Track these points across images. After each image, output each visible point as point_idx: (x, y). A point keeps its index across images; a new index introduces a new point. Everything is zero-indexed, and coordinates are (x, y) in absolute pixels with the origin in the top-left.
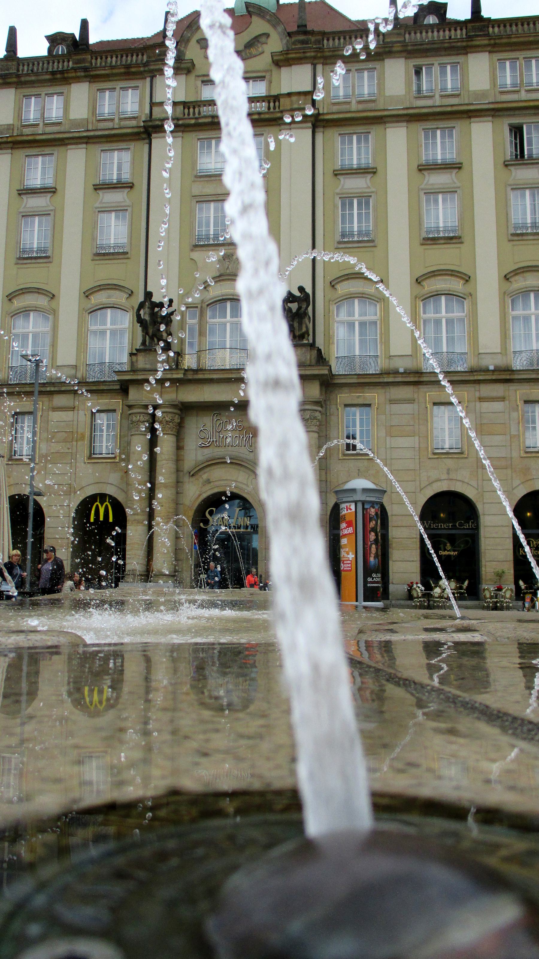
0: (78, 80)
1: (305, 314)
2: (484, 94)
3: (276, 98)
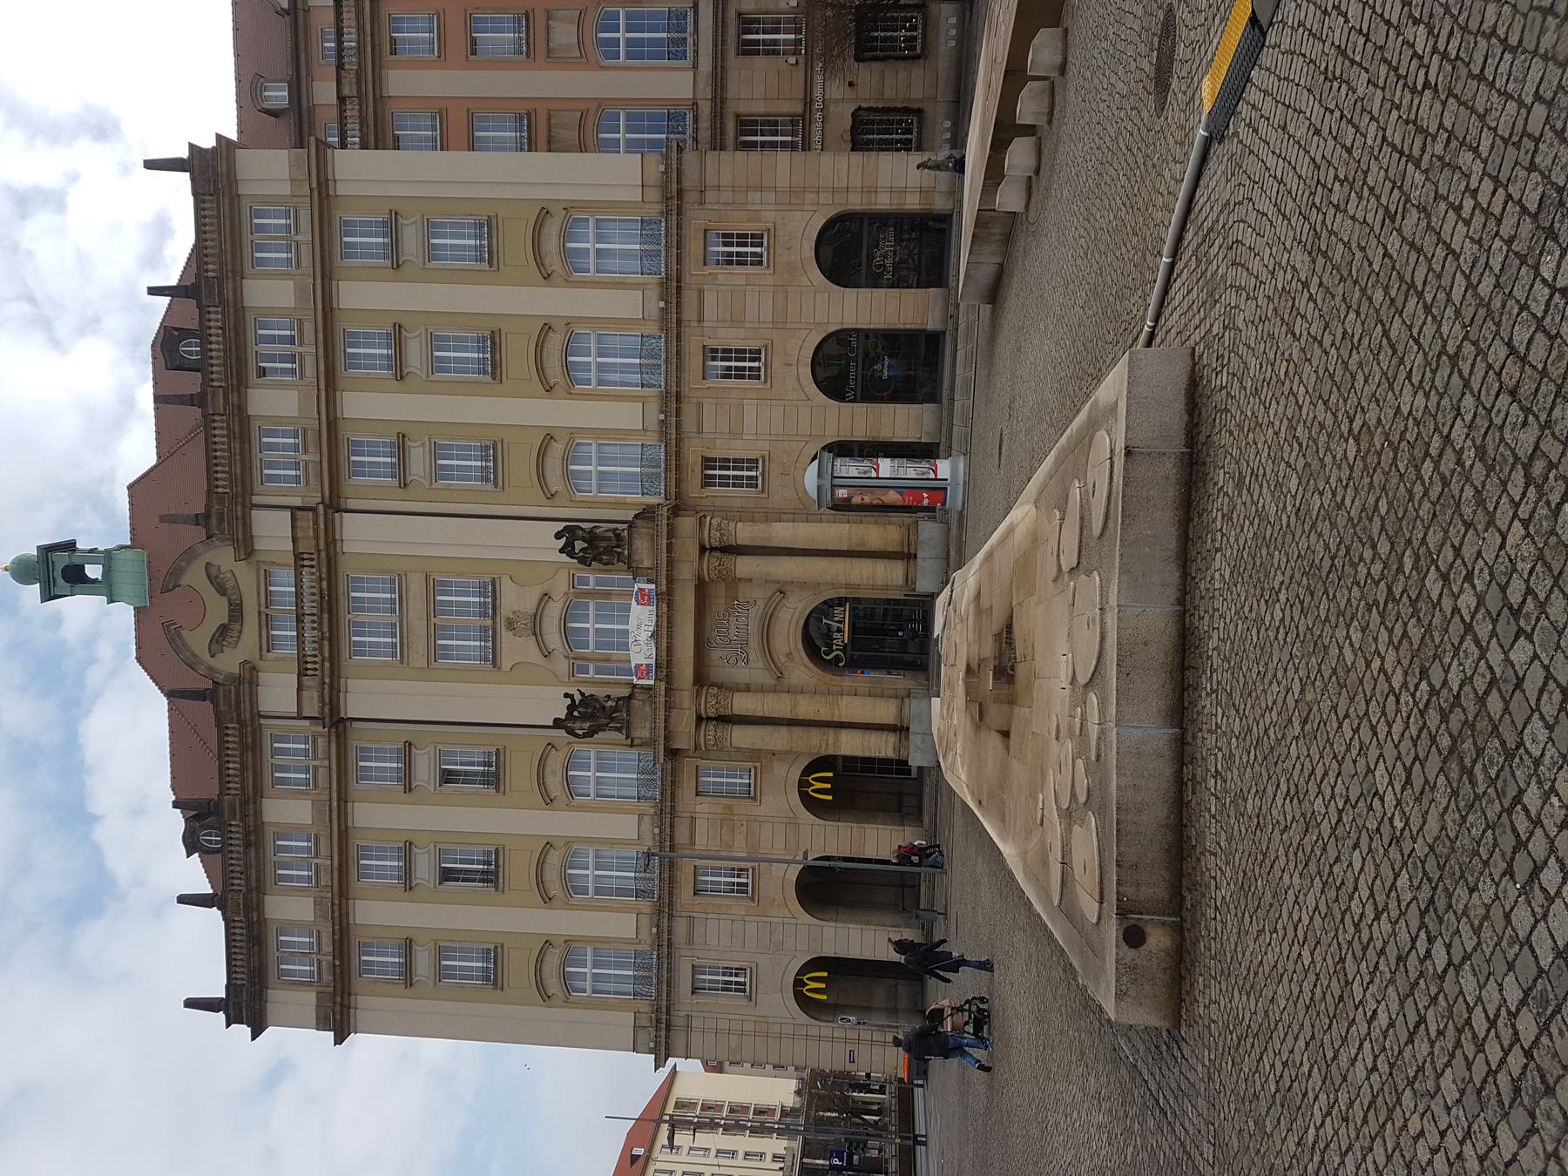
0: (258, 813)
1: (591, 531)
2: (299, 289)
3: (298, 556)
